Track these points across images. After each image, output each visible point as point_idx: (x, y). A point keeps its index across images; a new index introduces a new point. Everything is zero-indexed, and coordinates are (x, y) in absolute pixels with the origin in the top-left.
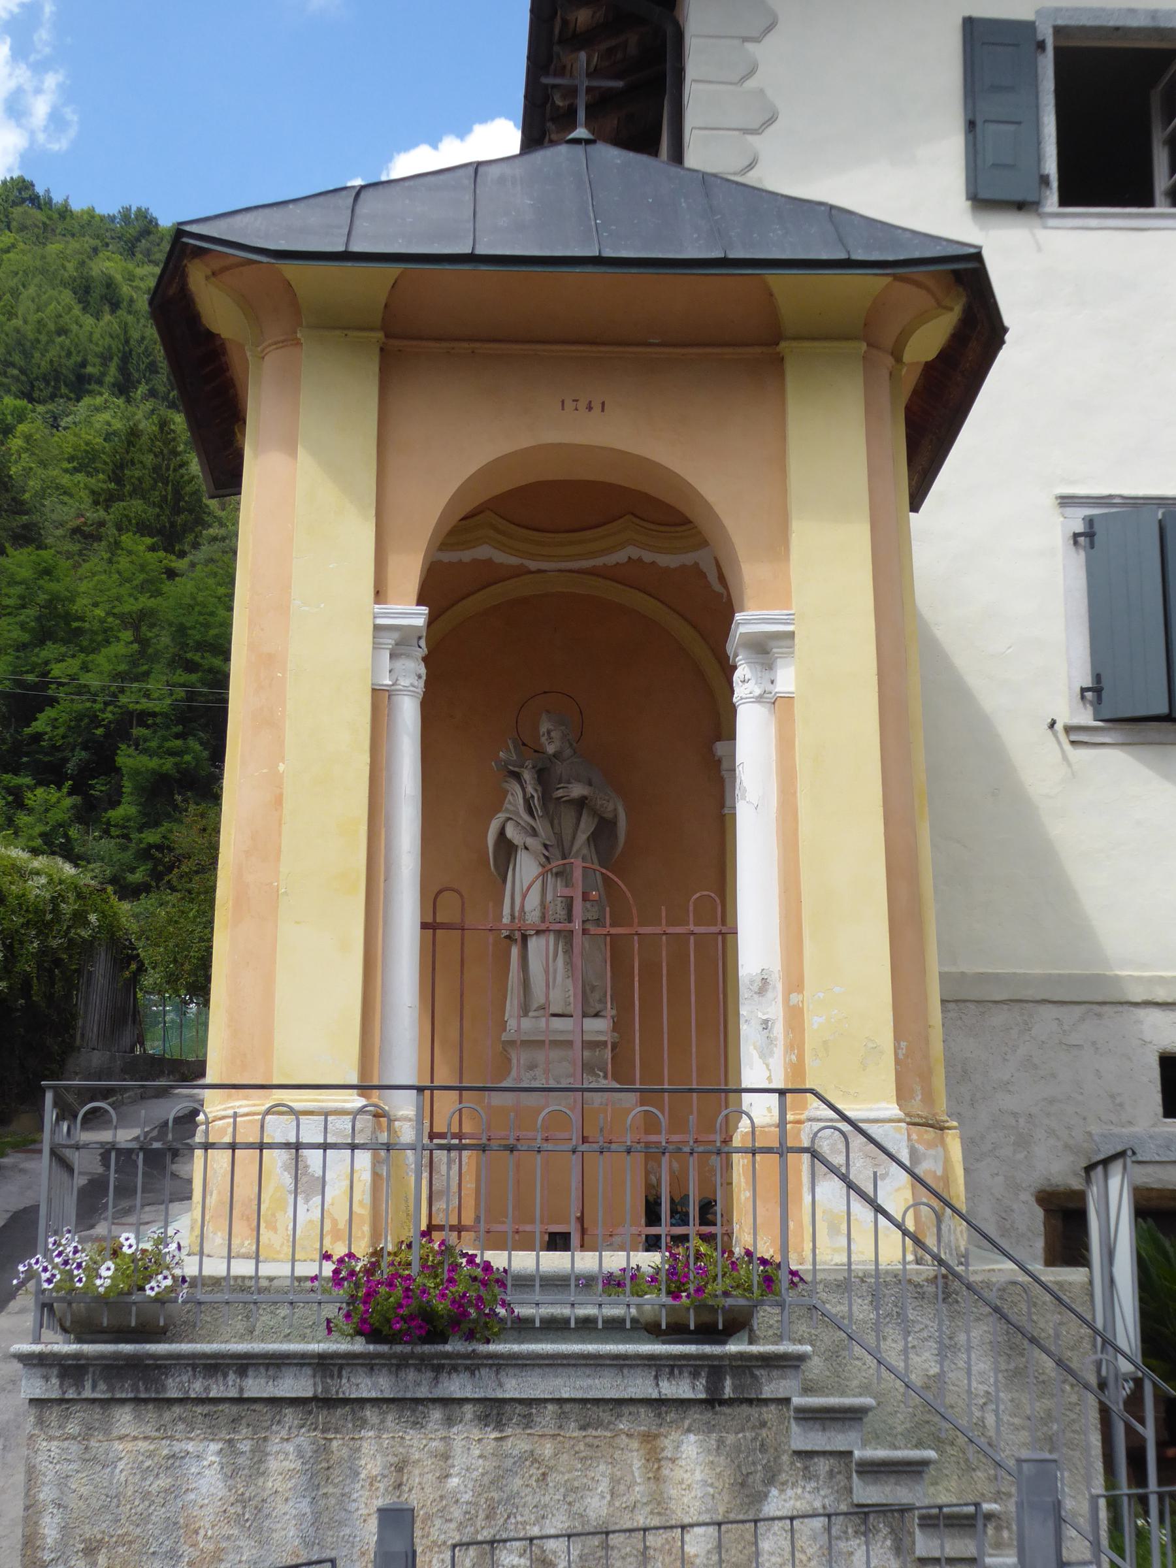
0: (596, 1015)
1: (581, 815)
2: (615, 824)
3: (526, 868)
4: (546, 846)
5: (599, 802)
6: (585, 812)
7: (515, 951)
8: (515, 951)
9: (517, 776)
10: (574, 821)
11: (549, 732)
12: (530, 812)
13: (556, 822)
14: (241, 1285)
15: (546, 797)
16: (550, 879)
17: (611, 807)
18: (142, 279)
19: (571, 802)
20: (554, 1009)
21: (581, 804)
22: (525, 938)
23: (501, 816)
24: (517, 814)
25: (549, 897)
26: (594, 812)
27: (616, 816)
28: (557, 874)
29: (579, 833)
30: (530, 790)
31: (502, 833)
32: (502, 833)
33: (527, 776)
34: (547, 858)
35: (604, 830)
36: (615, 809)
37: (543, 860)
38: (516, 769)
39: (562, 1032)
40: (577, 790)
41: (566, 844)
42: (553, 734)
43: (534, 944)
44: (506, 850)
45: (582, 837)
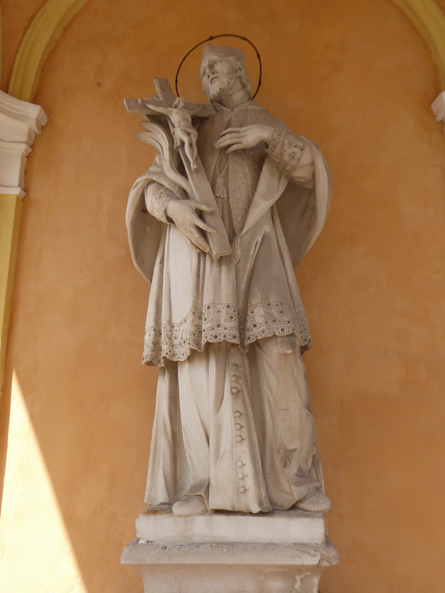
0: (294, 508)
1: (260, 170)
2: (312, 192)
3: (179, 256)
4: (200, 214)
5: (288, 150)
6: (265, 168)
7: (163, 386)
8: (163, 386)
9: (162, 121)
10: (249, 182)
11: (211, 66)
12: (180, 169)
13: (220, 181)
14: (265, 337)
15: (203, 147)
16: (210, 269)
17: (306, 158)
18: (185, 195)
19: (242, 152)
20: (215, 502)
21: (259, 156)
22: (172, 367)
23: (141, 180)
24: (162, 174)
25: (207, 299)
26: (281, 170)
27: (314, 177)
28: (221, 260)
29: (257, 198)
30: (179, 134)
31: (142, 209)
32: (142, 209)
33: (176, 117)
34: (203, 233)
35: (296, 200)
36: (313, 163)
37: (196, 236)
38: (161, 110)
39: (231, 545)
40: (252, 135)
41: (237, 214)
42: (218, 67)
43: (184, 374)
44: (149, 232)
45: (262, 206)
